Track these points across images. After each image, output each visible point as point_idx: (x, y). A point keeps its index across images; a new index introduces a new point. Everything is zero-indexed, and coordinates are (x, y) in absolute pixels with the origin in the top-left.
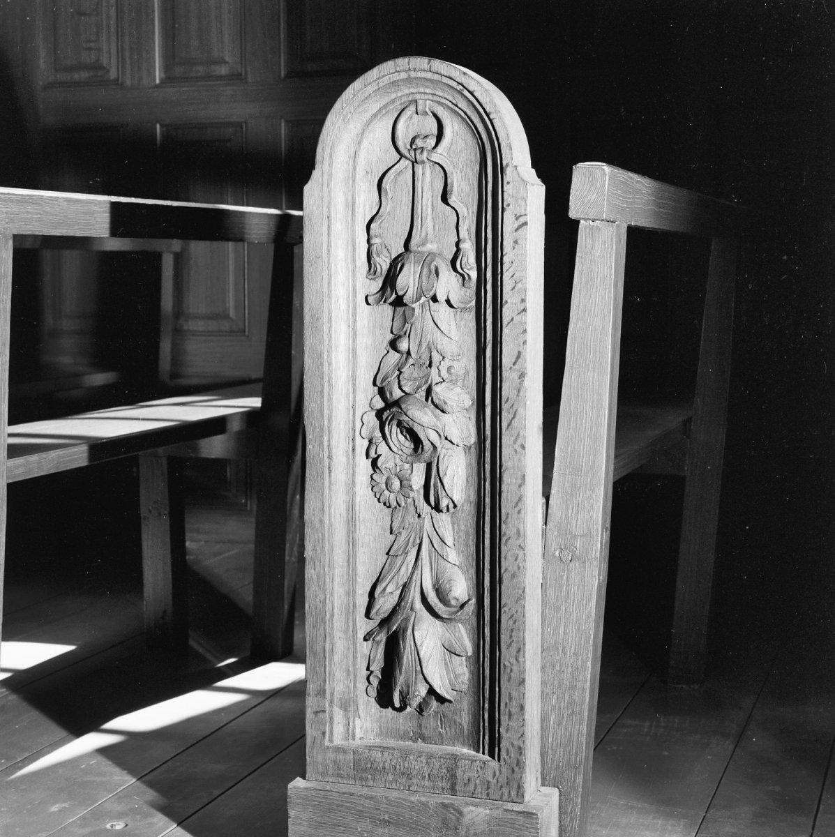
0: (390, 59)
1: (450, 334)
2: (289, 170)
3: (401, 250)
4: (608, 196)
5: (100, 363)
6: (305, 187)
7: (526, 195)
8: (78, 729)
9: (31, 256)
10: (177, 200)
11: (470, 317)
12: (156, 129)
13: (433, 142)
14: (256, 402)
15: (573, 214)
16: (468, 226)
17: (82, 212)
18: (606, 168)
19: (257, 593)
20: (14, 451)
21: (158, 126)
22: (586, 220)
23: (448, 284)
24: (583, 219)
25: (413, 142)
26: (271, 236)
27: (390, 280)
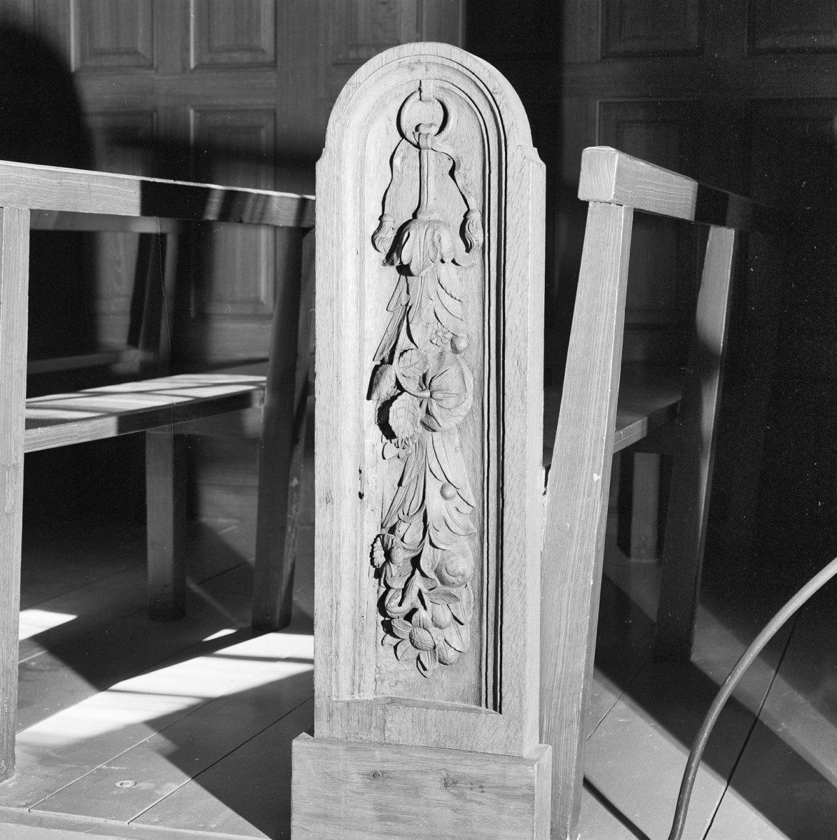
2: (297, 161)
3: (375, 545)
4: (616, 181)
9: (61, 253)
12: (188, 114)
13: (435, 130)
15: (582, 196)
16: (475, 203)
20: (31, 424)
21: (192, 112)
25: (417, 128)
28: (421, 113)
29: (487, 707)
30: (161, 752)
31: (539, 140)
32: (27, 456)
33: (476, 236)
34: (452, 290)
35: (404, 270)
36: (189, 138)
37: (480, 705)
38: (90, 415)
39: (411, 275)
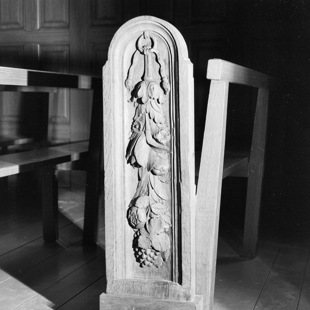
0: (143, 15)
1: (159, 111)
2: (95, 63)
4: (221, 72)
5: (22, 133)
6: (104, 67)
10: (51, 71)
12: (37, 46)
15: (208, 77)
17: (17, 77)
19: (85, 225)
21: (38, 46)
22: (213, 80)
23: (157, 92)
24: (213, 80)
26: (89, 84)
27: (134, 93)
29: (175, 282)
30: (49, 306)
31: (193, 56)
33: (167, 86)
36: (37, 54)
37: (172, 281)
39: (143, 104)
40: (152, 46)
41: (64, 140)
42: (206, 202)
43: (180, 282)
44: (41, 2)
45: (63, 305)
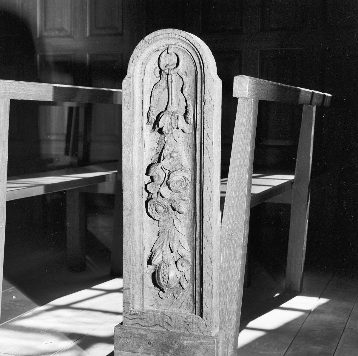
2: (118, 72)
7: (214, 85)
8: (42, 304)
9: (20, 110)
11: (190, 137)
14: (116, 171)
15: (234, 95)
18: (247, 77)
23: (181, 122)
24: (249, 189)
28: (168, 60)
31: (220, 73)
32: (7, 202)
34: (180, 146)
35: (161, 131)
38: (35, 186)
40: (177, 65)
41: (242, 276)
42: (165, 232)
43: (201, 316)
44: (41, 1)
45: (209, 172)
